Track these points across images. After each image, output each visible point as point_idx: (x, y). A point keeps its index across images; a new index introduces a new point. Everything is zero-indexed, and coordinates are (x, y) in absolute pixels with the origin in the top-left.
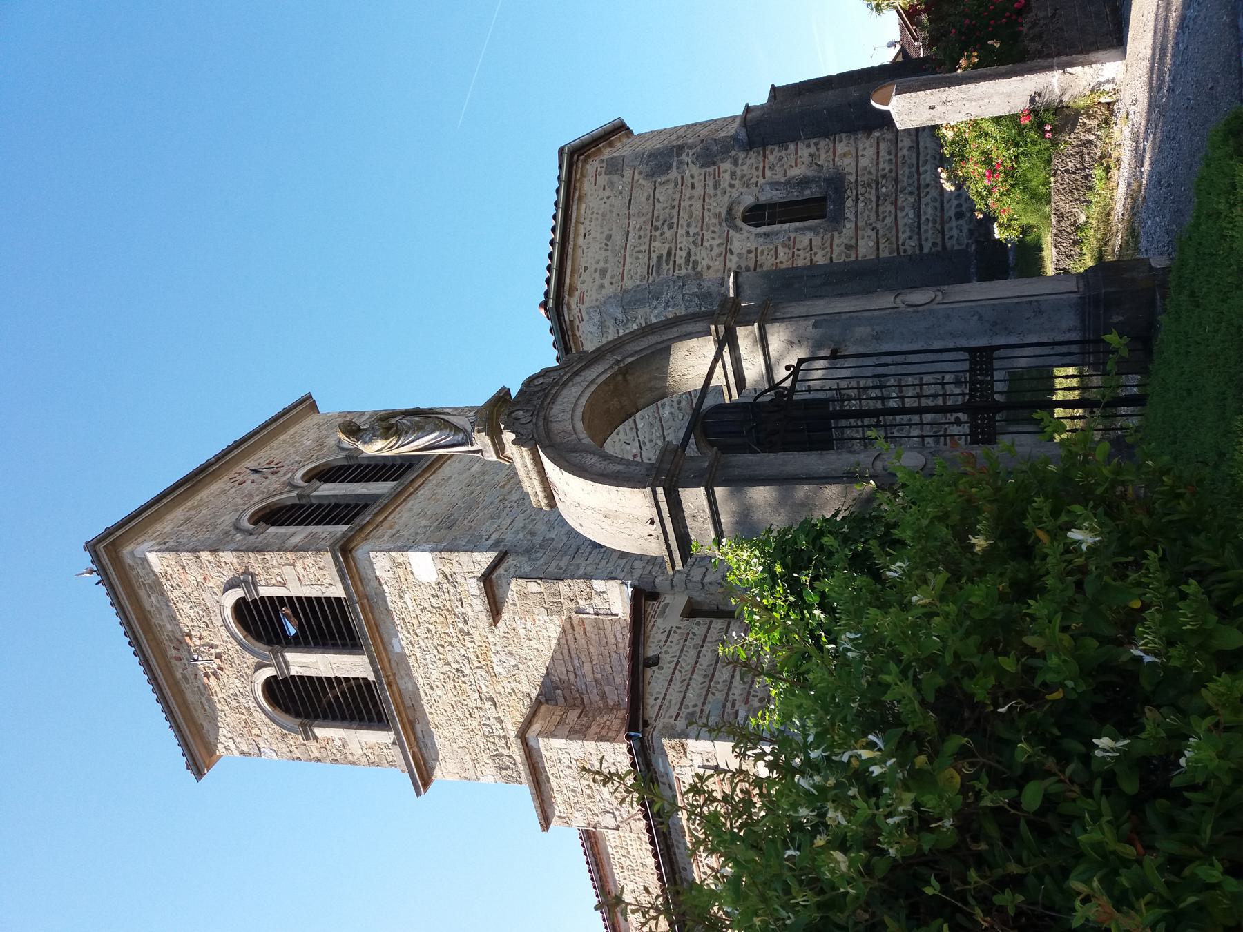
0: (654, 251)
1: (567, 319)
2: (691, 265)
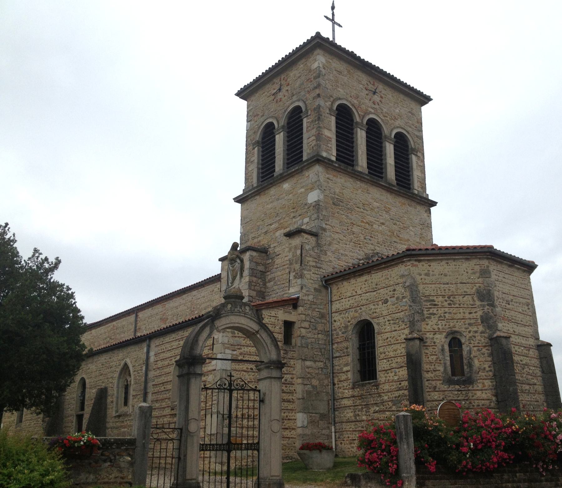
0: (437, 298)
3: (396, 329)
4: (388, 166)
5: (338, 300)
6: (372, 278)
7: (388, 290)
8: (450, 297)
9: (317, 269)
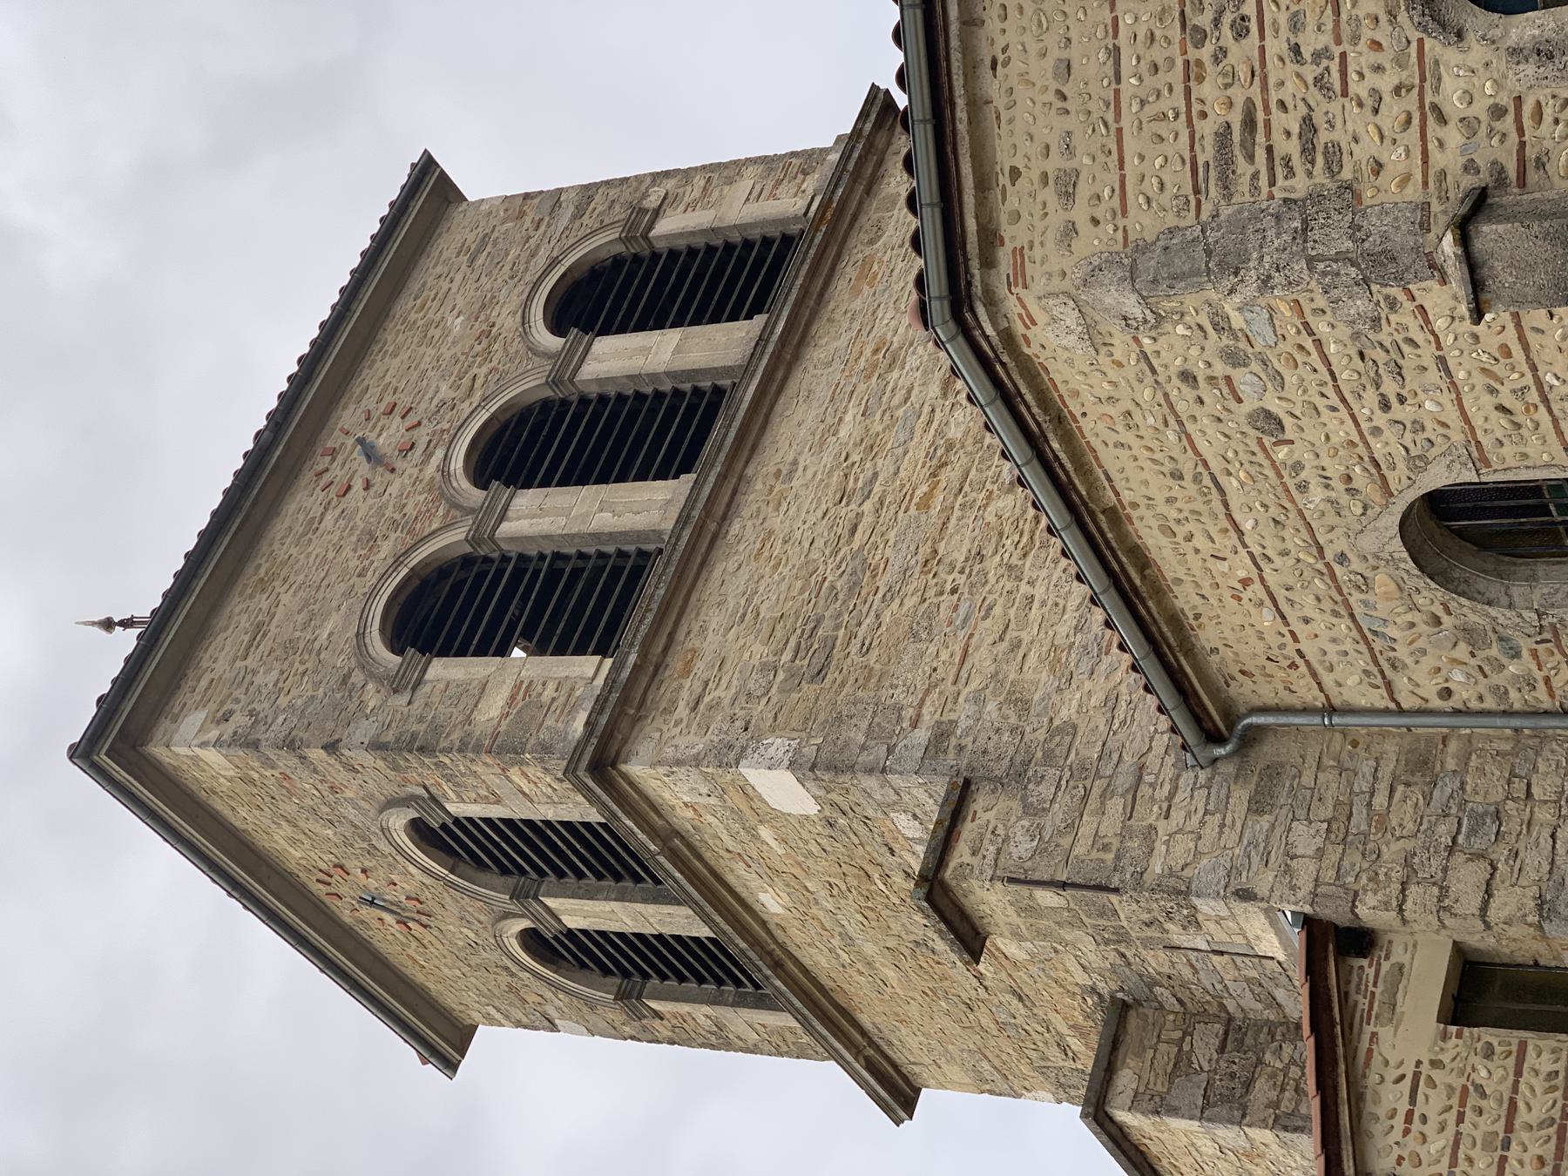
0: (1204, 115)
1: (990, 331)
2: (1320, 160)
3: (1428, 361)
4: (682, 363)
5: (1314, 674)
6: (1142, 502)
7: (1197, 410)
8: (1196, 28)
9: (1145, 790)
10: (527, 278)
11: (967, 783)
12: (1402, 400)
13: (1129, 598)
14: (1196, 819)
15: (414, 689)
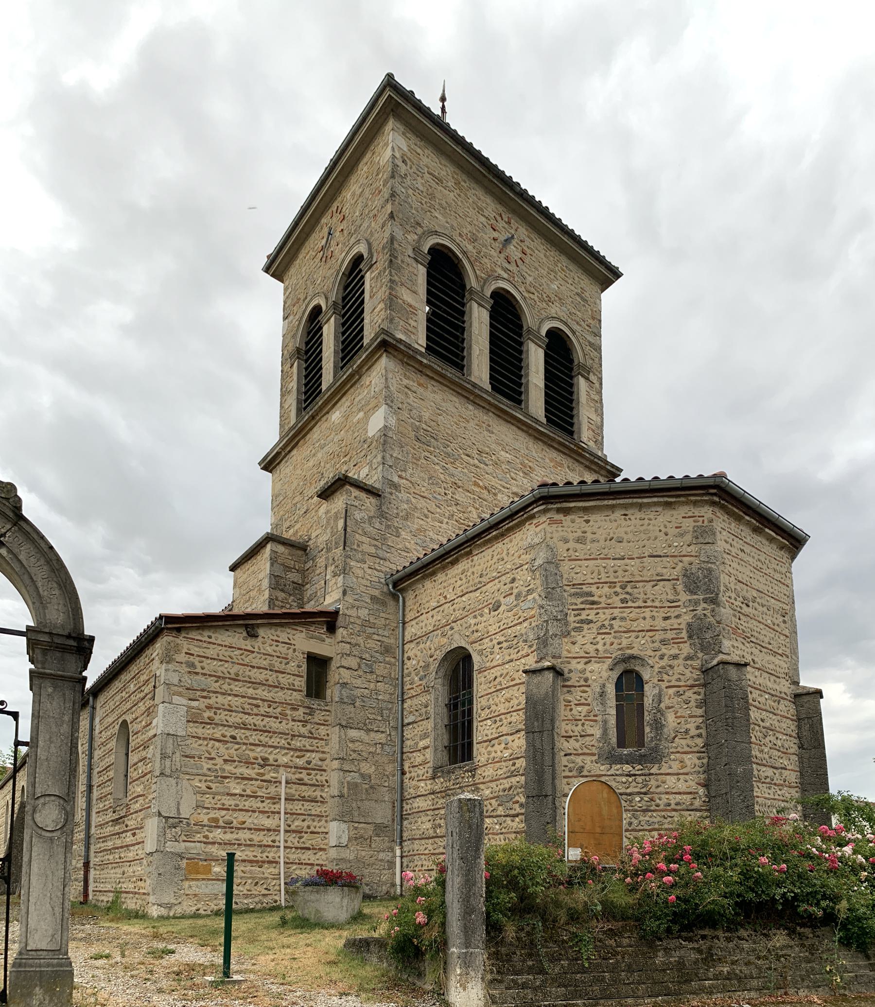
0: (598, 588)
1: (535, 510)
2: (578, 625)
3: (512, 657)
4: (531, 388)
5: (415, 618)
6: (473, 564)
7: (502, 583)
8: (626, 586)
9: (378, 560)
10: (569, 320)
11: (380, 496)
12: (500, 648)
13: (442, 557)
14: (369, 577)
15: (414, 258)
